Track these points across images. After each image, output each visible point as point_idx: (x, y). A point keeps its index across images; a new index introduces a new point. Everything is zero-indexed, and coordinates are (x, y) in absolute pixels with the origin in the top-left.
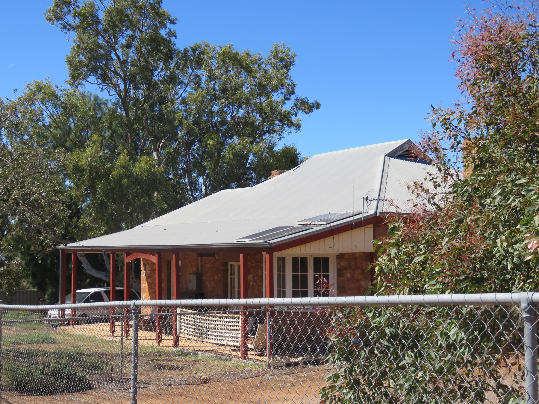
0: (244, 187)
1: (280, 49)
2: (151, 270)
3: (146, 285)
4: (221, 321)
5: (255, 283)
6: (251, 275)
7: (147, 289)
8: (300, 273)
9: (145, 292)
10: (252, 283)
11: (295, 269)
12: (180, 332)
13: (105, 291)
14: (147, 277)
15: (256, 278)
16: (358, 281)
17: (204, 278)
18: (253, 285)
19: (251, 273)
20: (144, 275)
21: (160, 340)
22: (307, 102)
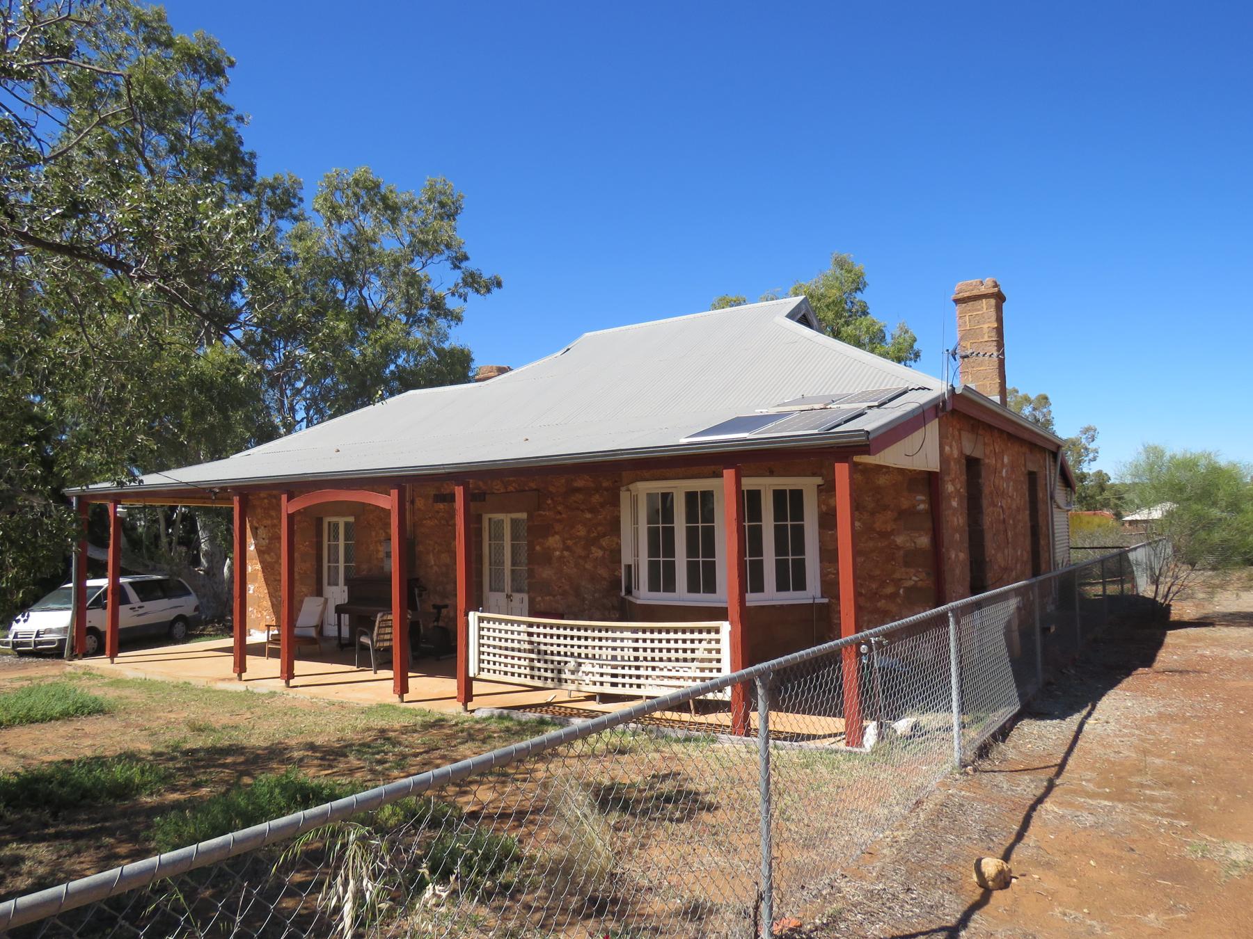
0: (452, 383)
1: (439, 187)
2: (270, 539)
3: (259, 567)
4: (572, 638)
5: (566, 553)
6: (557, 537)
7: (260, 575)
8: (789, 523)
9: (254, 581)
10: (558, 553)
11: (779, 514)
12: (481, 670)
13: (130, 583)
14: (260, 552)
15: (569, 542)
16: (884, 535)
17: (420, 548)
18: (562, 557)
19: (556, 533)
20: (252, 548)
21: (403, 689)
22: (480, 276)
